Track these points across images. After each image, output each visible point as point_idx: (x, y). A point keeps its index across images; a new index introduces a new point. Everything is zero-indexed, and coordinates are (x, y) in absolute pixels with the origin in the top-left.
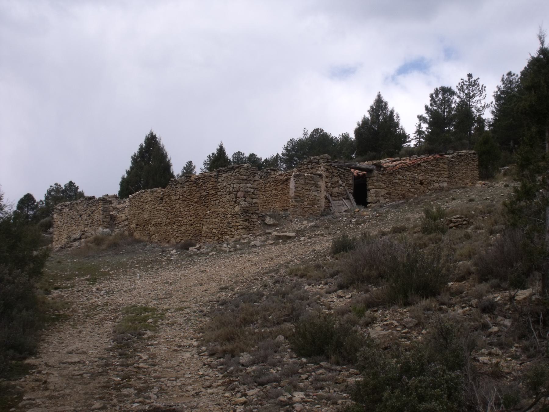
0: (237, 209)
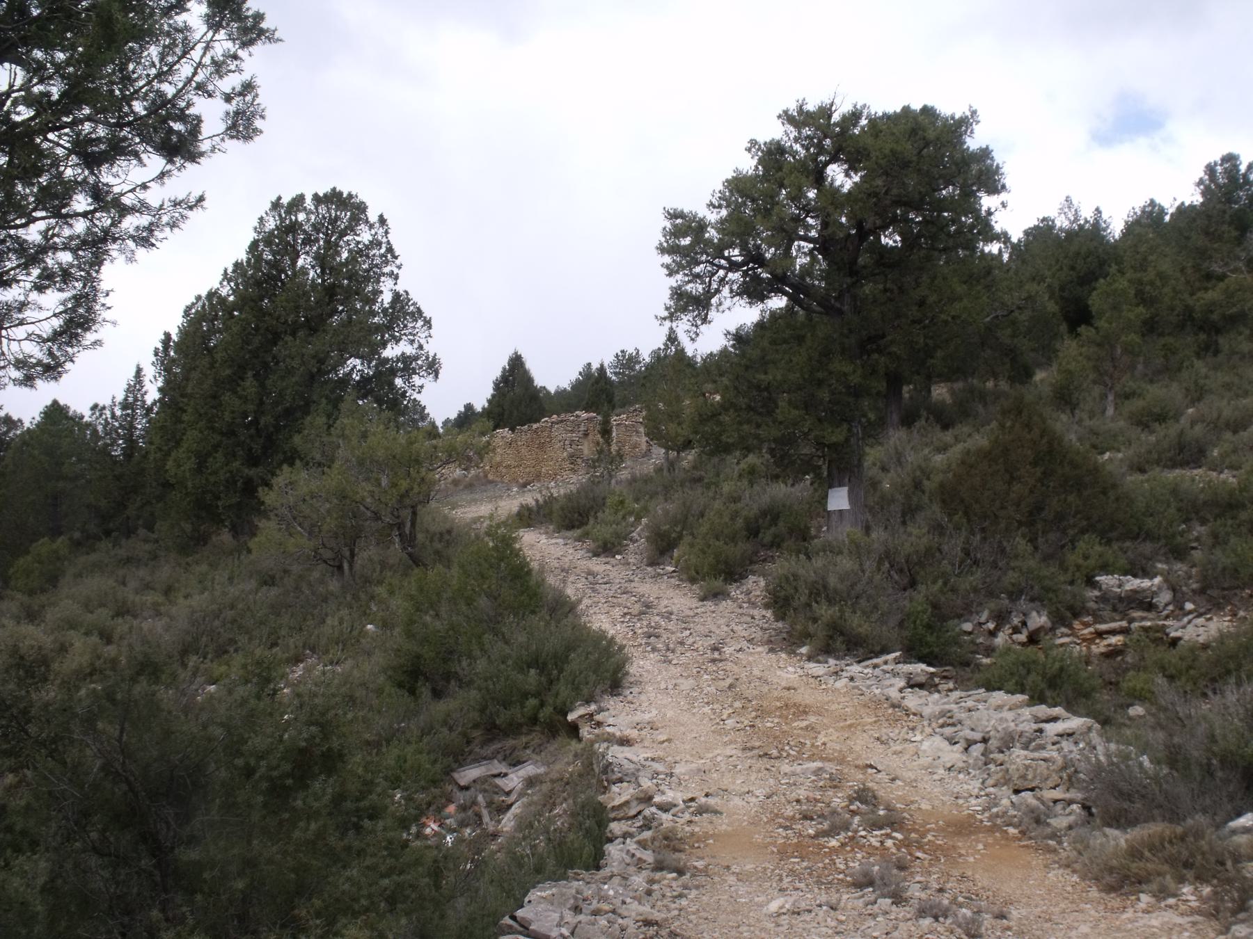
0: (565, 454)
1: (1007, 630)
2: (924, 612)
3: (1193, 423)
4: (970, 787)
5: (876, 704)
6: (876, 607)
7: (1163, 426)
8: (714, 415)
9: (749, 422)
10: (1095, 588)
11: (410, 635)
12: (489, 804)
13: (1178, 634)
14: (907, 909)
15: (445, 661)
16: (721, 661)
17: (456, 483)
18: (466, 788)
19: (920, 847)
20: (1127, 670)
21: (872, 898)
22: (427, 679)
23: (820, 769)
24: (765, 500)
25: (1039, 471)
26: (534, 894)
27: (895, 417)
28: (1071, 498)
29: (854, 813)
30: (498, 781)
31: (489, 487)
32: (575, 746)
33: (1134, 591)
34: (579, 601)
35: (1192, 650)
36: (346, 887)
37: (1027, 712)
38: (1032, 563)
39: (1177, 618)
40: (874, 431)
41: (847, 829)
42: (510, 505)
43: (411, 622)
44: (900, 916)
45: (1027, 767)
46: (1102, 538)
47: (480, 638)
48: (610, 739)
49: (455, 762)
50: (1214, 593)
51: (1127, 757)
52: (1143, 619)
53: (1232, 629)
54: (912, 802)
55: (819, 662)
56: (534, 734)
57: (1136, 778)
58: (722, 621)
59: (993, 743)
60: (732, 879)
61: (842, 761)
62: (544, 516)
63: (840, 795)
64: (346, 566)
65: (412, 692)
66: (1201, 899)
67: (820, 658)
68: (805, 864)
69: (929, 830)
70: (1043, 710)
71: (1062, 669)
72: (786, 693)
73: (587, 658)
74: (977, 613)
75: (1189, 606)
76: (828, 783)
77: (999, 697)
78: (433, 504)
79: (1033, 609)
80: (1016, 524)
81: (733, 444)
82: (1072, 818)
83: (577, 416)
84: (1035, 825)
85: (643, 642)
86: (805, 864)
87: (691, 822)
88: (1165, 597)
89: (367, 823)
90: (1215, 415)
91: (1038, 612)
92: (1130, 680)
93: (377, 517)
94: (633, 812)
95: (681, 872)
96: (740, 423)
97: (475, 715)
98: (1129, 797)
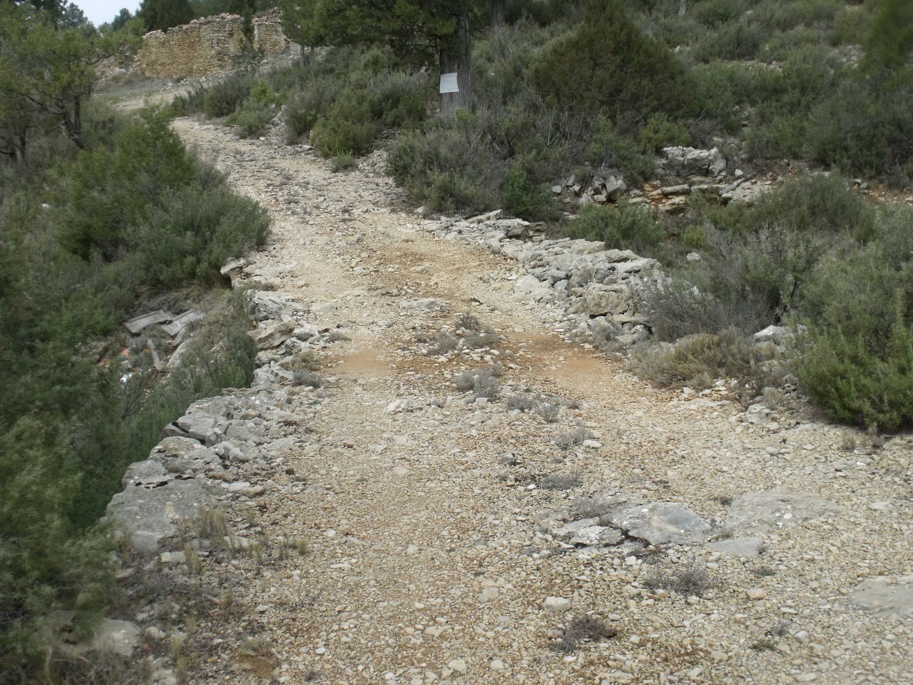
0: (213, 52)
1: (590, 191)
2: (521, 176)
3: (749, 22)
4: (556, 314)
5: (480, 252)
6: (480, 173)
7: (726, 23)
8: (340, 11)
9: (370, 16)
10: (663, 157)
11: (79, 208)
12: (158, 347)
13: (729, 195)
14: (500, 404)
15: (113, 229)
16: (350, 220)
17: (116, 79)
18: (138, 335)
19: (513, 360)
20: (688, 224)
21: (472, 398)
22: (97, 245)
23: (432, 303)
24: (388, 85)
25: (618, 59)
26: (193, 407)
27: (500, 16)
28: (645, 82)
29: (460, 336)
30: (165, 328)
31: (146, 83)
32: (228, 294)
33: (695, 160)
34: (228, 174)
35: (740, 207)
36: (22, 390)
37: (602, 255)
38: (611, 136)
39: (728, 182)
40: (481, 25)
41: (454, 348)
42: (167, 96)
43: (80, 196)
44: (494, 410)
45: (601, 297)
46: (669, 116)
47: (142, 207)
48: (257, 286)
49: (127, 314)
50: (759, 161)
51: (679, 287)
52: (701, 182)
53: (771, 191)
54: (508, 327)
55: (432, 219)
56: (193, 287)
57: (686, 302)
58: (352, 188)
59: (575, 279)
60: (358, 389)
61: (451, 296)
62: (197, 106)
63: (448, 323)
64: (18, 154)
65: (86, 257)
66: (730, 389)
67: (434, 216)
68: (419, 375)
69: (521, 347)
70: (615, 253)
71: (634, 222)
72: (405, 244)
73: (235, 220)
74: (565, 178)
75: (739, 172)
76: (439, 314)
77: (581, 243)
78: (95, 95)
79: (612, 174)
80: (598, 103)
81: (357, 36)
82: (636, 336)
83: (223, 18)
84: (605, 341)
85: (284, 207)
86: (419, 375)
87: (325, 347)
88: (720, 165)
89: (38, 344)
90: (769, 16)
91: (615, 177)
92: (689, 232)
93: (43, 108)
94: (277, 343)
95: (316, 386)
96: (363, 17)
97: (142, 274)
98: (680, 317)
